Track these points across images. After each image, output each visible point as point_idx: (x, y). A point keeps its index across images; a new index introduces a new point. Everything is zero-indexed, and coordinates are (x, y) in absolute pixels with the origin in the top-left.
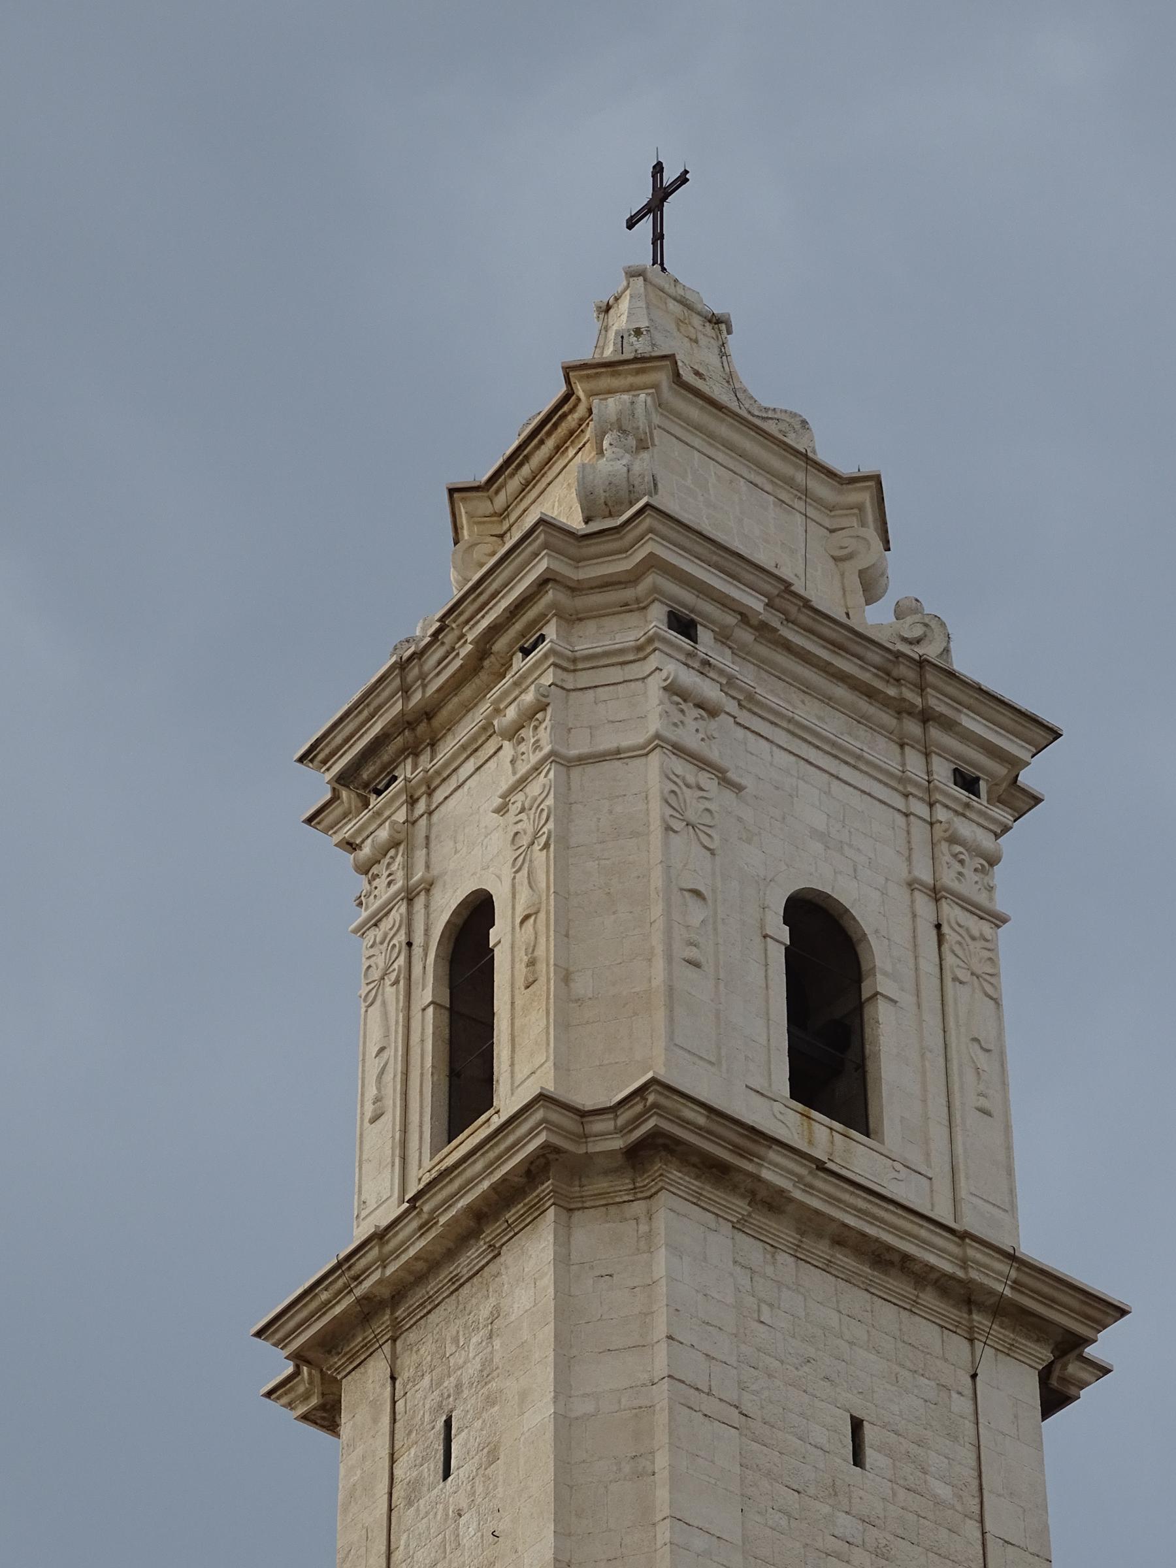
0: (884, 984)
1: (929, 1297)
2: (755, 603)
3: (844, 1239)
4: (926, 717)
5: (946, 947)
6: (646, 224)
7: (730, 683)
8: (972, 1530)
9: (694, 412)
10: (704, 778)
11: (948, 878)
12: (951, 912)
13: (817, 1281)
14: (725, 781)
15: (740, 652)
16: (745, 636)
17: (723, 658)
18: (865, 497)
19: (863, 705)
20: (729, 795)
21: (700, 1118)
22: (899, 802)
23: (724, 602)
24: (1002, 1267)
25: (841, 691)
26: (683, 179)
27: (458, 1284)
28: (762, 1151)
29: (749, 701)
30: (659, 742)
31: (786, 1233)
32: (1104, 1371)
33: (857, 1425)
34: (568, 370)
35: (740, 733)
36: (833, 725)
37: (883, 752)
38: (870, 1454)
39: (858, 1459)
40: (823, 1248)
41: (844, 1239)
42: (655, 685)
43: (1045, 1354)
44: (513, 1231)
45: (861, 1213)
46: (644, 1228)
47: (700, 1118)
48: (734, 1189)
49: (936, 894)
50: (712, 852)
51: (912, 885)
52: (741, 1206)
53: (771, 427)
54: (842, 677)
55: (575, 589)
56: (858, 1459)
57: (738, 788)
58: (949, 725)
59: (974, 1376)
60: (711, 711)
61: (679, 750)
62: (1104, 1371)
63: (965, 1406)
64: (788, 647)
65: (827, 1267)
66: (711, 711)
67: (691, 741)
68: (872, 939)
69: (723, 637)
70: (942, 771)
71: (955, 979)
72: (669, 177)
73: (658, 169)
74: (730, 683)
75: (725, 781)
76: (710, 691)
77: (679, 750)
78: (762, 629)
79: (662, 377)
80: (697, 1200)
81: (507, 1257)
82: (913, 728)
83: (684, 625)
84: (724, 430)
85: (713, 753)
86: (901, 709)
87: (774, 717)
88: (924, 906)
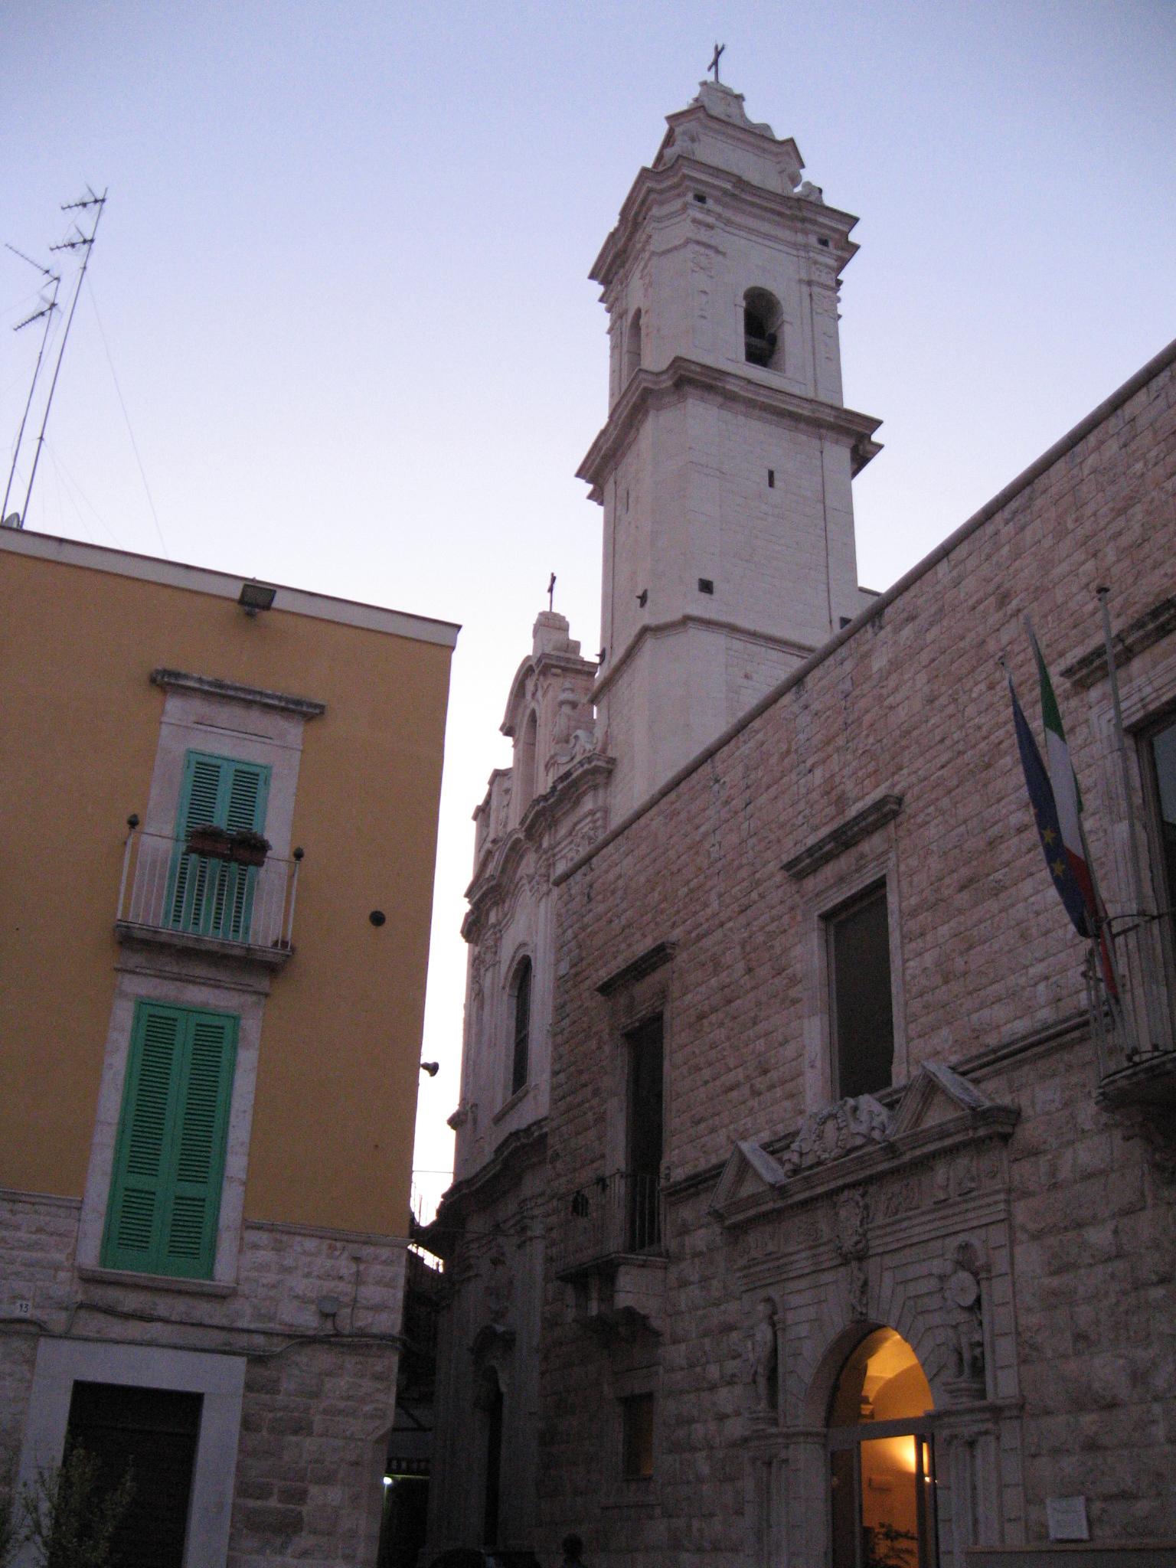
0: (786, 317)
1: (802, 426)
2: (728, 186)
3: (765, 408)
4: (804, 220)
5: (813, 303)
6: (713, 69)
7: (719, 217)
8: (820, 506)
9: (716, 126)
10: (707, 252)
11: (815, 277)
12: (816, 290)
13: (756, 425)
14: (717, 251)
15: (725, 206)
16: (728, 199)
17: (719, 209)
18: (790, 149)
19: (777, 218)
20: (720, 258)
21: (698, 369)
22: (795, 253)
23: (714, 186)
24: (828, 411)
25: (768, 215)
26: (723, 48)
27: (630, 445)
28: (722, 377)
29: (729, 222)
30: (688, 241)
31: (741, 408)
32: (880, 447)
33: (771, 474)
34: (670, 119)
35: (726, 234)
36: (766, 227)
37: (787, 234)
38: (776, 483)
39: (771, 484)
40: (757, 412)
41: (765, 408)
42: (689, 221)
43: (852, 442)
44: (642, 422)
45: (768, 397)
46: (683, 412)
47: (698, 369)
48: (716, 393)
49: (810, 283)
50: (711, 277)
51: (800, 281)
52: (720, 400)
53: (757, 131)
54: (766, 209)
55: (661, 192)
56: (771, 484)
57: (724, 254)
58: (814, 222)
59: (822, 452)
60: (710, 227)
61: (698, 243)
62: (880, 447)
63: (819, 463)
64: (744, 201)
65: (759, 419)
66: (710, 227)
67: (704, 239)
68: (782, 302)
69: (717, 201)
70: (813, 240)
71: (817, 313)
72: (719, 48)
73: (716, 47)
74: (719, 217)
75: (717, 251)
76: (710, 220)
77: (698, 243)
78: (733, 196)
79: (701, 115)
80: (702, 399)
81: (641, 431)
82: (799, 225)
83: (701, 198)
84: (730, 131)
85: (713, 242)
86: (793, 218)
87: (740, 227)
88: (805, 289)
